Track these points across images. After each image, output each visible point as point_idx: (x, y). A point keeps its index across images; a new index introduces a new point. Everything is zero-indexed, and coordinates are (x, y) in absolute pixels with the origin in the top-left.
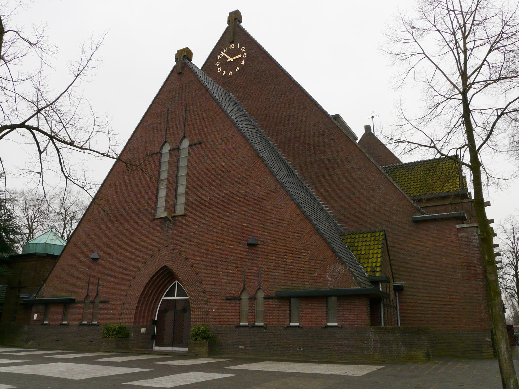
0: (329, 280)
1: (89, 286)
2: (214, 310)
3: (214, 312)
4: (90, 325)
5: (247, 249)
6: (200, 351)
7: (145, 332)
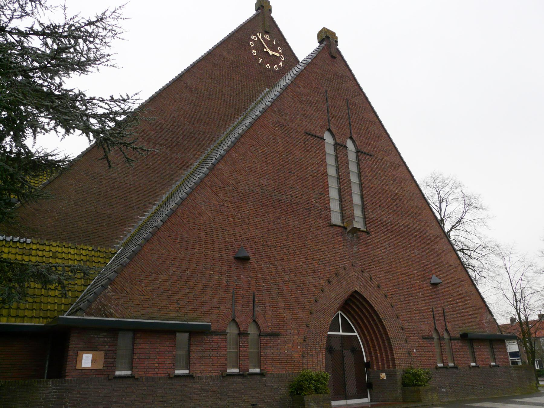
0: (485, 326)
1: (233, 304)
2: (415, 351)
3: (415, 353)
4: (445, 367)
5: (431, 288)
6: (433, 398)
7: (381, 379)
